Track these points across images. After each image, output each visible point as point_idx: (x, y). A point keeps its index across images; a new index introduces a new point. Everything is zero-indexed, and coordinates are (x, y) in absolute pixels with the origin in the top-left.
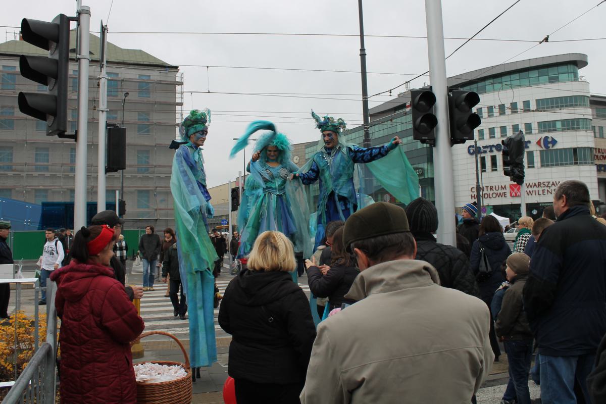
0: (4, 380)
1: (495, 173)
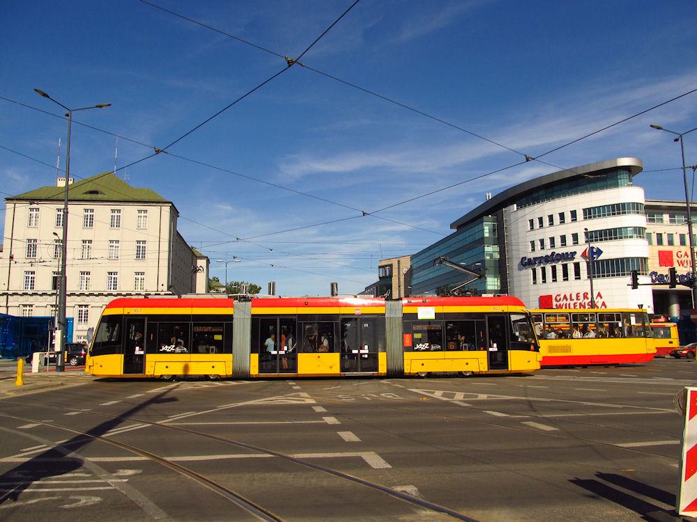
0: (192, 301)
1: (566, 282)
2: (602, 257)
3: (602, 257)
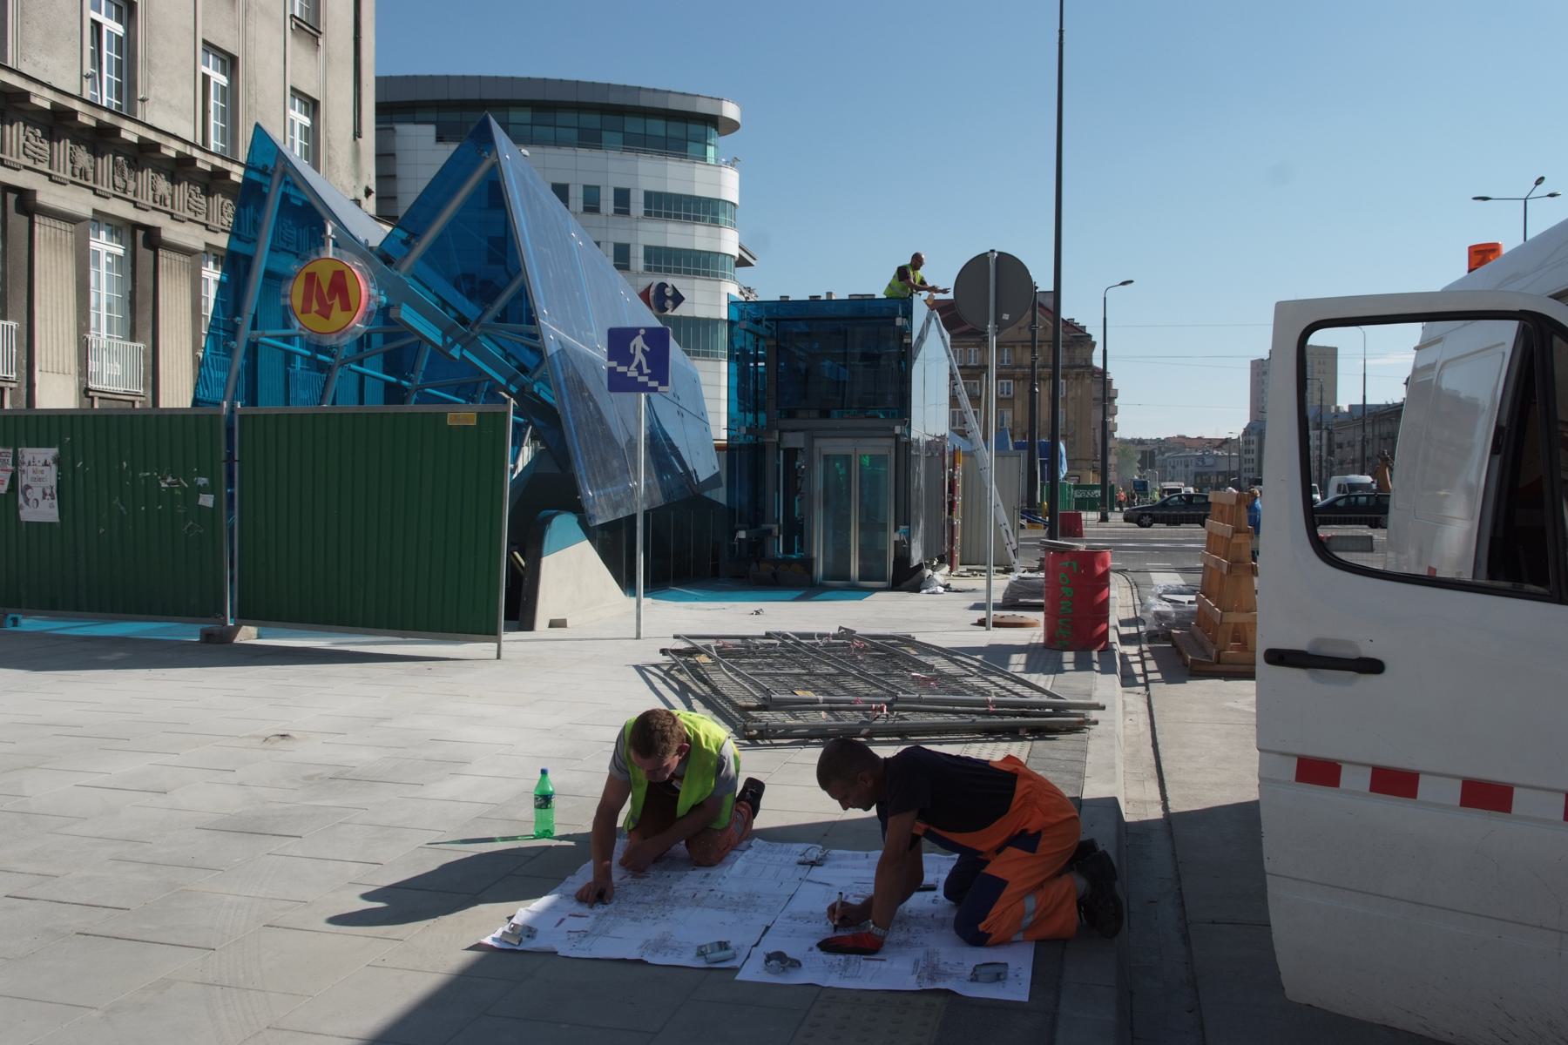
2: (682, 310)
3: (682, 310)
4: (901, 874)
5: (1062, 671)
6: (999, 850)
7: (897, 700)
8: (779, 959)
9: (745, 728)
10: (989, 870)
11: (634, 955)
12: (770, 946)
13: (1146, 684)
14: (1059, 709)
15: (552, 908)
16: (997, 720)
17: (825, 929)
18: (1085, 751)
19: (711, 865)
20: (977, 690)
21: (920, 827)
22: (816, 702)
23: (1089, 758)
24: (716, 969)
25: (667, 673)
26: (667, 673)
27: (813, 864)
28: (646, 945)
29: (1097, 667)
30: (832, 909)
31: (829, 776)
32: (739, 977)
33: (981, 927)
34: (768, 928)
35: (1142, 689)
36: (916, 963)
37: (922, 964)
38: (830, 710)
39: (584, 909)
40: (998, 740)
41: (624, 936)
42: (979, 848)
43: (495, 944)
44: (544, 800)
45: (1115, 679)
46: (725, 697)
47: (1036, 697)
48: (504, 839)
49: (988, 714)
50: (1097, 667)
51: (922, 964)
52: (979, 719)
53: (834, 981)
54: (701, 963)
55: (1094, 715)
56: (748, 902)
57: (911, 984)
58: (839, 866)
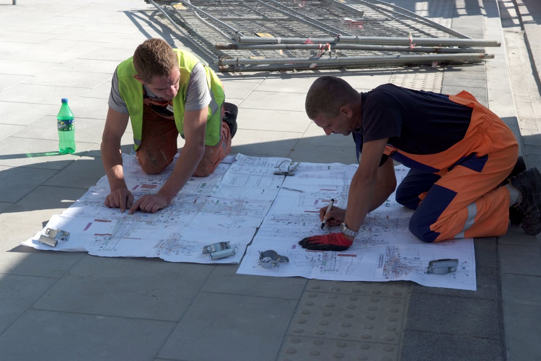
4: (371, 188)
5: (458, 16)
6: (450, 168)
7: (338, 40)
8: (271, 257)
9: (220, 63)
10: (439, 183)
11: (152, 254)
12: (263, 244)
13: (522, 25)
14: (464, 47)
15: (77, 216)
16: (416, 56)
17: (313, 228)
18: (485, 80)
19: (206, 176)
20: (393, 31)
21: (389, 149)
22: (276, 42)
23: (489, 85)
24: (219, 266)
25: (151, 17)
26: (151, 17)
27: (286, 174)
28: (160, 245)
29: (483, 12)
30: (323, 211)
31: (316, 106)
32: (240, 271)
33: (432, 227)
34: (258, 229)
35: (518, 29)
36: (381, 258)
37: (385, 259)
38: (285, 49)
39: (108, 213)
40: (416, 71)
41: (143, 238)
42: (436, 167)
43: (36, 246)
44: (66, 124)
45: (497, 21)
46: (200, 37)
47: (443, 37)
48: (34, 155)
49: (408, 51)
50: (483, 12)
51: (385, 259)
52: (403, 56)
53: (316, 274)
54: (207, 260)
55: (489, 50)
56: (239, 207)
57: (379, 276)
58: (307, 176)
